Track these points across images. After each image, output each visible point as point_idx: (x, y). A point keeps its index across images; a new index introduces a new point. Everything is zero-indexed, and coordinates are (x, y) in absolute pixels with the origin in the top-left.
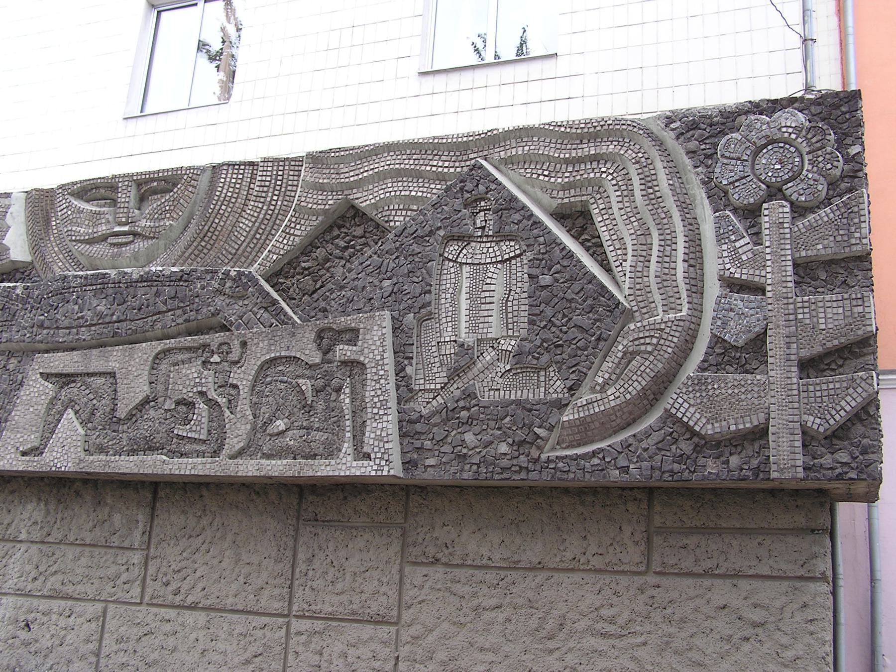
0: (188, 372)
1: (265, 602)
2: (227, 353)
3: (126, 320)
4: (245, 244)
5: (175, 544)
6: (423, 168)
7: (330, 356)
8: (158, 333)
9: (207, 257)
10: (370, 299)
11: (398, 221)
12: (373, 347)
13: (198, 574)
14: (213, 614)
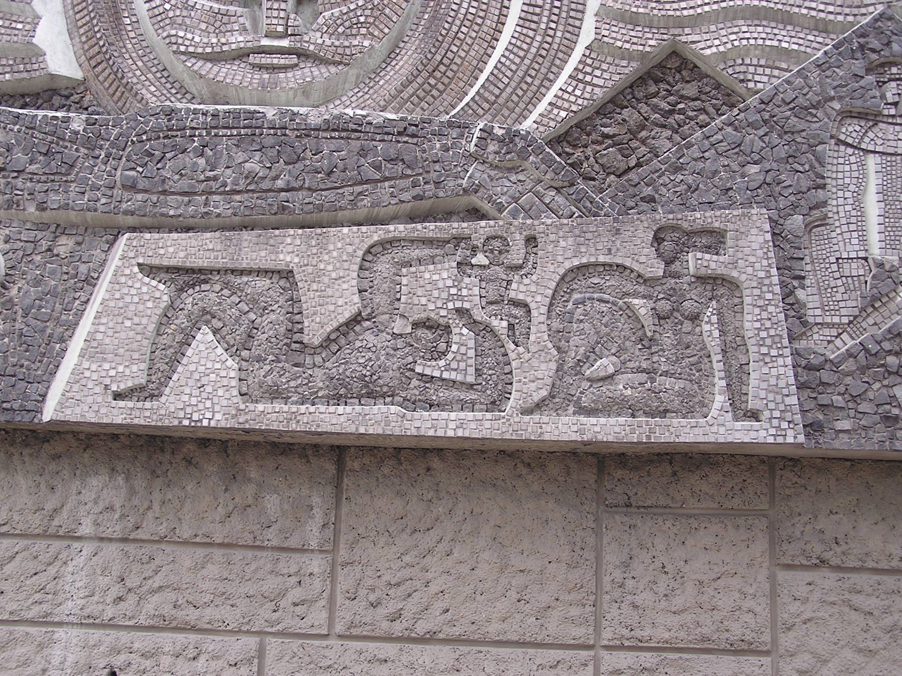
0: (436, 277)
1: (553, 628)
2: (500, 252)
3: (301, 188)
4: (509, 90)
5: (387, 544)
7: (676, 267)
8: (361, 213)
9: (437, 102)
10: (728, 190)
11: (764, 82)
13: (434, 588)
14: (464, 649)
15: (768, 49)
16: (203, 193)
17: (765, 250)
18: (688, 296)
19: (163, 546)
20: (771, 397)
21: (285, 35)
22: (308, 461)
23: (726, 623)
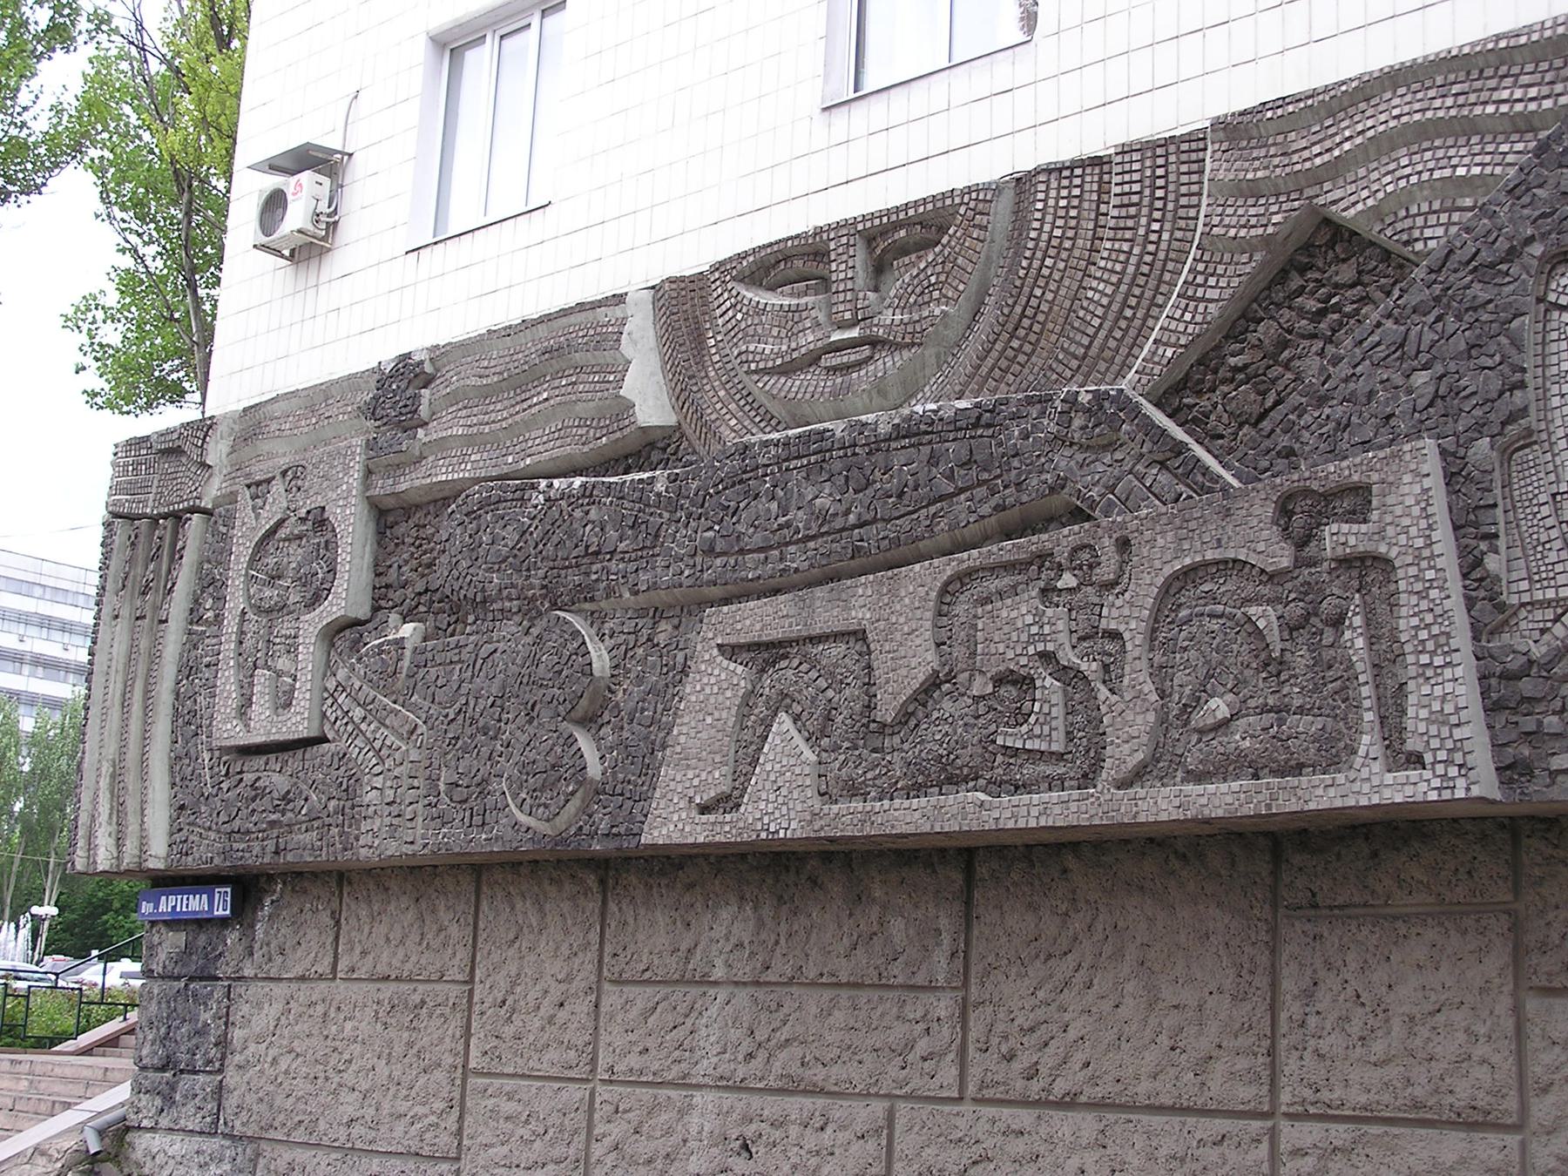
0: (1014, 614)
1: (1217, 1087)
3: (875, 521)
5: (1019, 975)
6: (1478, 110)
7: (1311, 550)
8: (943, 539)
9: (1026, 371)
10: (1388, 417)
11: (1433, 237)
12: (1406, 521)
13: (1072, 1034)
15: (1438, 184)
16: (779, 545)
17: (1423, 505)
18: (1328, 592)
19: (794, 989)
20: (1433, 730)
21: (854, 323)
22: (934, 871)
23: (1448, 1080)
